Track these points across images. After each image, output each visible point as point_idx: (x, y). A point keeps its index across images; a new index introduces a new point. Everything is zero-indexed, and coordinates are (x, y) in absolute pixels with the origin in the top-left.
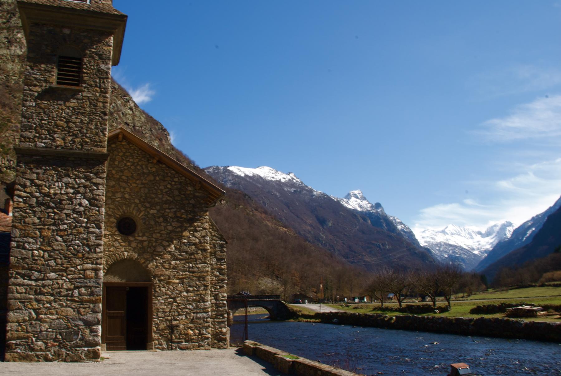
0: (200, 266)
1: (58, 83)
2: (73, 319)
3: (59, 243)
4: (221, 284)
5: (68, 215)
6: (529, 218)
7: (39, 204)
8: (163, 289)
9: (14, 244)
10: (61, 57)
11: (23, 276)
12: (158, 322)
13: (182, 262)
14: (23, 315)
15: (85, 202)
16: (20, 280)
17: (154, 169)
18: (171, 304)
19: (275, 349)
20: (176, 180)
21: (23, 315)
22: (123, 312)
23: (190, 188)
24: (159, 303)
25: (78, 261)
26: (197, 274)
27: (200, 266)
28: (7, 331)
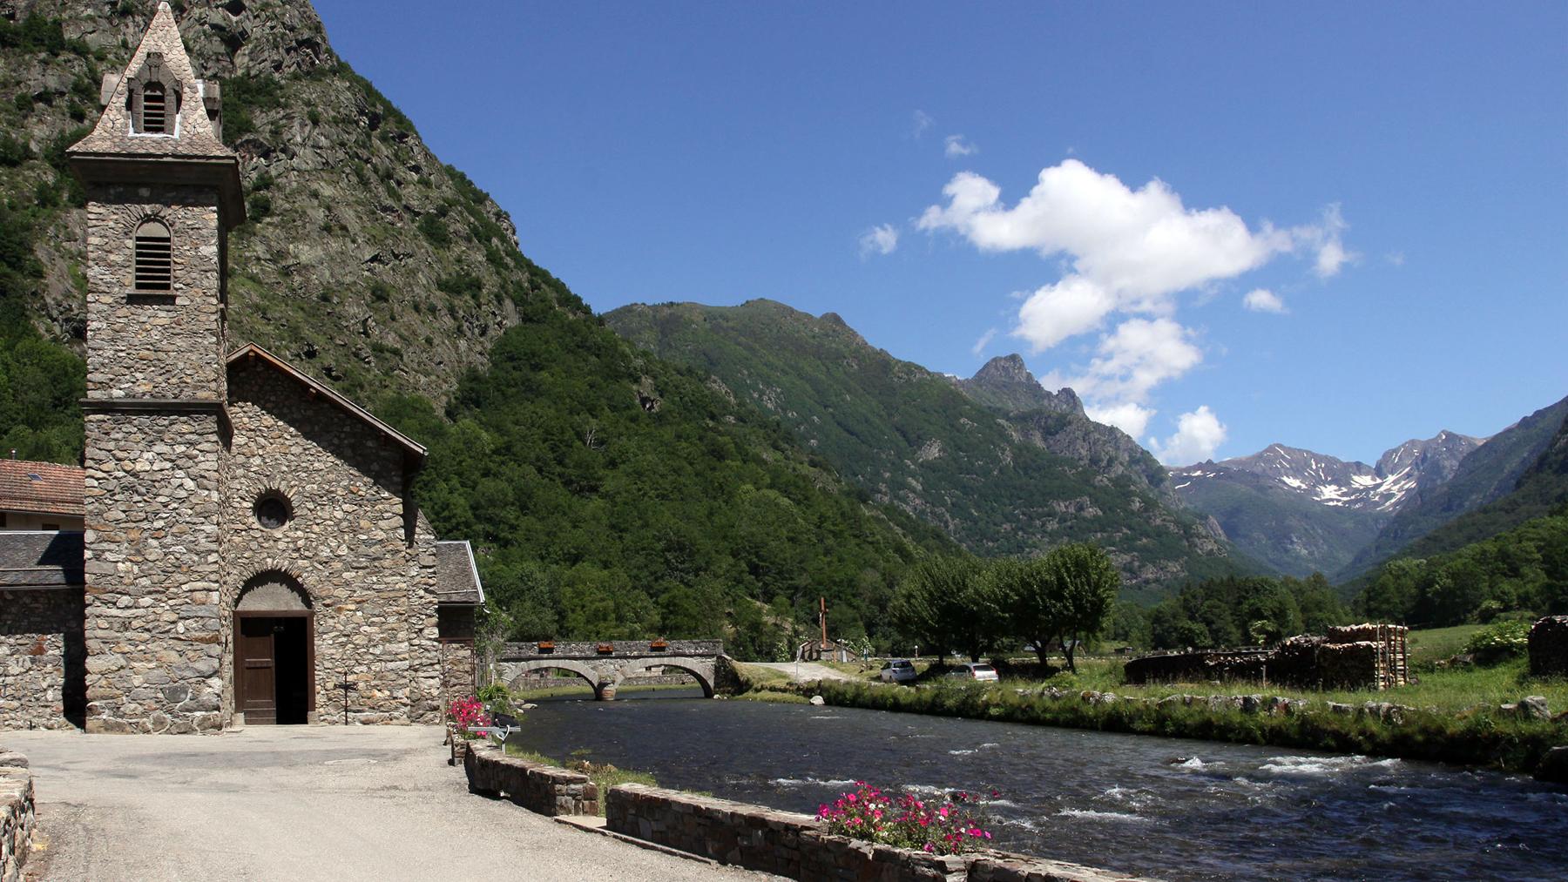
0: (388, 580)
1: (139, 286)
2: (179, 668)
3: (154, 550)
4: (1420, 790)
5: (165, 505)
6: (1512, 420)
7: (125, 489)
8: (331, 622)
9: (88, 554)
10: (138, 239)
11: (105, 603)
12: (324, 679)
13: (361, 573)
14: (111, 661)
15: (190, 484)
16: (104, 610)
17: (310, 413)
18: (343, 645)
19: (727, 802)
20: (347, 429)
21: (111, 661)
22: (268, 660)
23: (370, 444)
24: (324, 646)
25: (183, 578)
26: (385, 595)
27: (388, 580)
28: (87, 688)
